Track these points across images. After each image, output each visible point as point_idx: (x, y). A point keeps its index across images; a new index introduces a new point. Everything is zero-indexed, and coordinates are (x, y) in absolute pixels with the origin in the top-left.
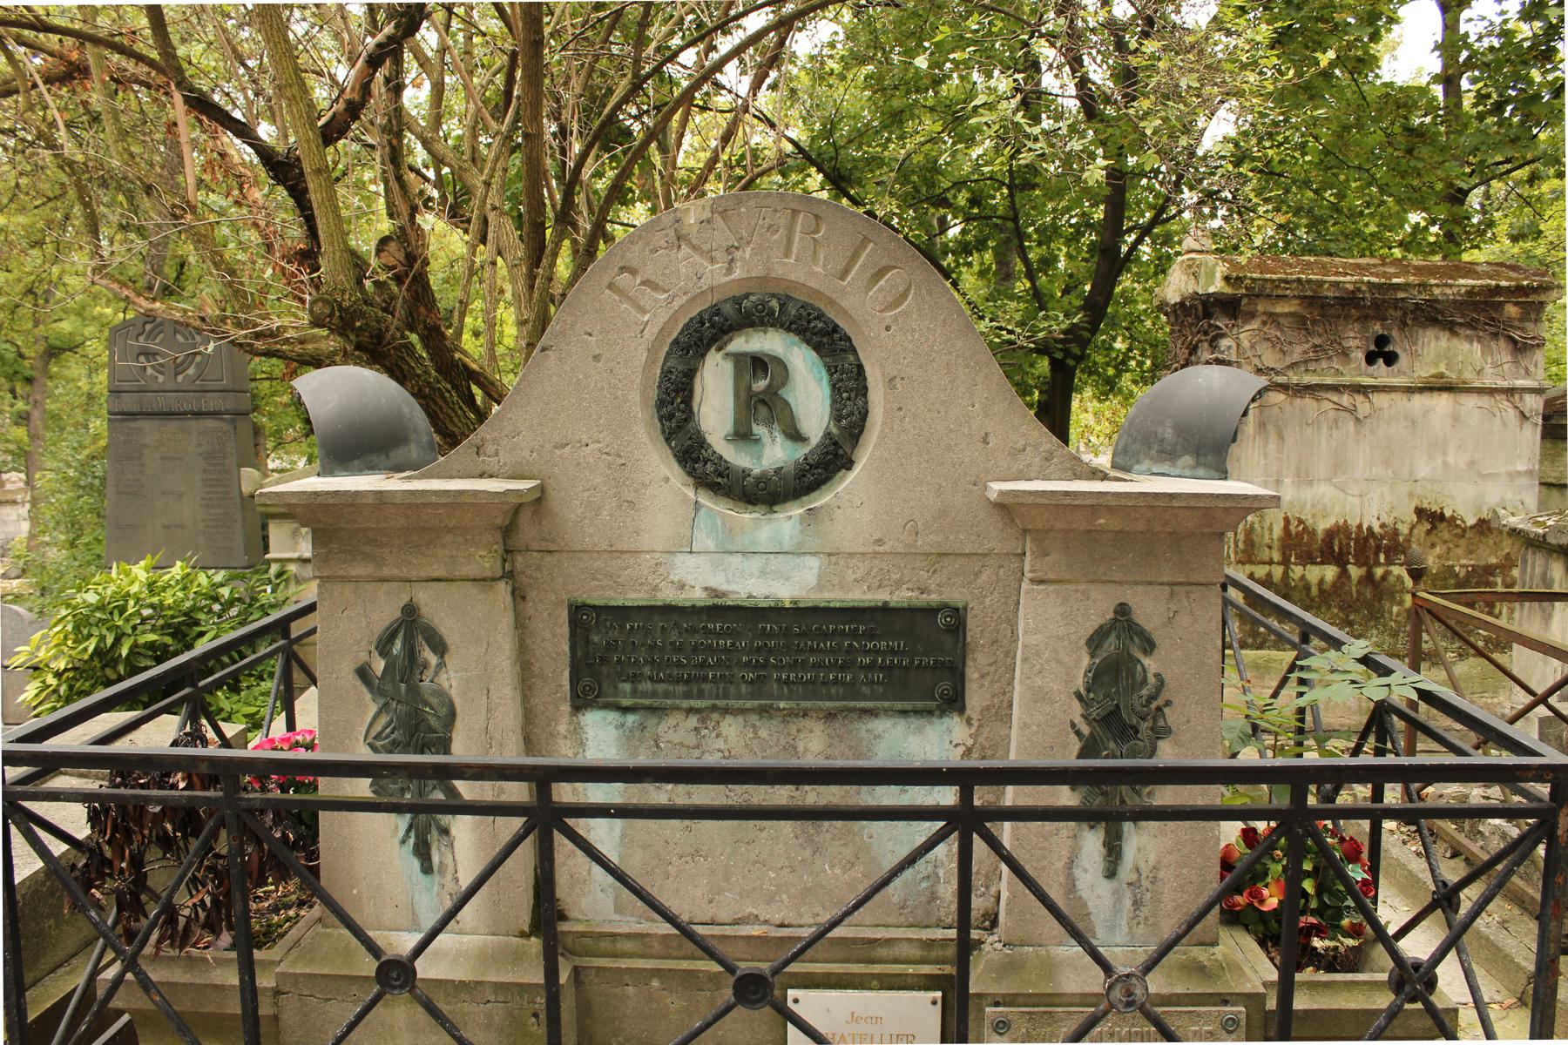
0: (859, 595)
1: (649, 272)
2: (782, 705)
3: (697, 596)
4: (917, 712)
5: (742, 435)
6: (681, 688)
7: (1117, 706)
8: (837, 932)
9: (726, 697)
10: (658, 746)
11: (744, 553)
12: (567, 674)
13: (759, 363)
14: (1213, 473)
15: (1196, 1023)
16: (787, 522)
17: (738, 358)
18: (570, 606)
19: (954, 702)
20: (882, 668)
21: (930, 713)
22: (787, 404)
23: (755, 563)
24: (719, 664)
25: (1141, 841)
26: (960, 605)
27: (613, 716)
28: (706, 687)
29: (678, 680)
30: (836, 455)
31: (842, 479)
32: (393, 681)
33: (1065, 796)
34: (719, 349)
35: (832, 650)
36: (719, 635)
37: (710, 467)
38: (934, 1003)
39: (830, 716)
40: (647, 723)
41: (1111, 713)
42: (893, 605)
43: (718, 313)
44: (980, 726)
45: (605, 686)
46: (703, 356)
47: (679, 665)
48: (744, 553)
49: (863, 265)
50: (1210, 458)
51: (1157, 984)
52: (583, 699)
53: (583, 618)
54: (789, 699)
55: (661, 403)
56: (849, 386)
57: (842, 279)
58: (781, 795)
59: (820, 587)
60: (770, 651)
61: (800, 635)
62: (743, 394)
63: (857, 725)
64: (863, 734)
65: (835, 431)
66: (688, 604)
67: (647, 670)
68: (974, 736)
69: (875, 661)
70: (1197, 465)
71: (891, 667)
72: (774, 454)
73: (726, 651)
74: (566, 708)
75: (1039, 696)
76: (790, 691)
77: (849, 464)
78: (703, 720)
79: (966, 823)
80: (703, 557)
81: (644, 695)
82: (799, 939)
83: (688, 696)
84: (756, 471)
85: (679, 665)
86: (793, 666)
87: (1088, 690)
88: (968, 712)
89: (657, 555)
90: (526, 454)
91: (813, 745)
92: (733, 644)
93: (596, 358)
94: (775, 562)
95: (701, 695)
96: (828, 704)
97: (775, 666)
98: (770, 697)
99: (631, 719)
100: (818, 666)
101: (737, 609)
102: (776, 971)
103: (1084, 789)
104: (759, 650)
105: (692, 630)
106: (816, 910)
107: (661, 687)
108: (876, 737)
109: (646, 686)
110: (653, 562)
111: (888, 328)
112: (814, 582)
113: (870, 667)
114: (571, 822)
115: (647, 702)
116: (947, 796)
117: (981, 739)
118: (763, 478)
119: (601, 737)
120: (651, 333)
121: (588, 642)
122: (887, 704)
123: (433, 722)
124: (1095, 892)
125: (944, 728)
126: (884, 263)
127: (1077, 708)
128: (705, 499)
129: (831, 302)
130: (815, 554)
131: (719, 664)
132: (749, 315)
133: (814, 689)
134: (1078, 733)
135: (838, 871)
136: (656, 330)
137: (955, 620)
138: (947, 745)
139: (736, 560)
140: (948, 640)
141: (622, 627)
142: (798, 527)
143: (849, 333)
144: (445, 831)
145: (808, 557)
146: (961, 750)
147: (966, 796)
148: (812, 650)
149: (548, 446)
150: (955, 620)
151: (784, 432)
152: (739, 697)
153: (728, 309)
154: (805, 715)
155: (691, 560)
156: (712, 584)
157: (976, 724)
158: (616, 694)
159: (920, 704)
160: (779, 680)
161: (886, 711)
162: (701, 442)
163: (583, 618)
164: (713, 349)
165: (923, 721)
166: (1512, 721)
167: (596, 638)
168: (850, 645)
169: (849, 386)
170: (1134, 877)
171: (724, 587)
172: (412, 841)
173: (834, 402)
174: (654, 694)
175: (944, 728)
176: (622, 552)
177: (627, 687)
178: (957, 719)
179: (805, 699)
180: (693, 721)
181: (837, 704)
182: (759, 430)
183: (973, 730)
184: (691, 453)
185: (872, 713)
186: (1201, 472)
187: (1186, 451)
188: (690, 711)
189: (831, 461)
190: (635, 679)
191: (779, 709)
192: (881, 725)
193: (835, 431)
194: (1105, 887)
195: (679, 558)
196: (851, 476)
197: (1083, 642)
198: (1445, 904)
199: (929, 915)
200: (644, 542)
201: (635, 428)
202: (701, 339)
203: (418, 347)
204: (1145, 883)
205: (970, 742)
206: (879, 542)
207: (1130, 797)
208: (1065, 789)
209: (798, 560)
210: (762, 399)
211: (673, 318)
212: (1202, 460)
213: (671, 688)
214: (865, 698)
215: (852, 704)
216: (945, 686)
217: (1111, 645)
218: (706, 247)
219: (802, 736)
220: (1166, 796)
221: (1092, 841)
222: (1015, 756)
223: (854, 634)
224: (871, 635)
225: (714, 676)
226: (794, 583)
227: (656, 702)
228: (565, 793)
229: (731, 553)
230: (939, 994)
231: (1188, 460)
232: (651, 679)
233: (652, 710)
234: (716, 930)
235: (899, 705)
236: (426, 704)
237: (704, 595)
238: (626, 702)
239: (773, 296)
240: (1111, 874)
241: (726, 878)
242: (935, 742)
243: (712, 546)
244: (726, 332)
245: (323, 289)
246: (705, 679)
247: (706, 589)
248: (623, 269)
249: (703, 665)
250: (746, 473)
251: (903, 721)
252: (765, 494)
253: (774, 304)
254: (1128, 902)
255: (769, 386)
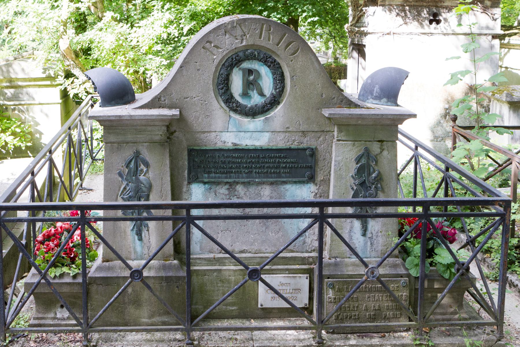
0: (281, 145)
1: (216, 43)
2: (257, 180)
3: (229, 146)
5: (245, 94)
6: (224, 175)
7: (365, 180)
8: (281, 255)
9: (238, 178)
11: (245, 132)
13: (250, 72)
14: (393, 104)
15: (393, 284)
16: (259, 122)
17: (244, 70)
18: (188, 150)
19: (312, 179)
20: (289, 168)
22: (259, 84)
23: (249, 134)
24: (237, 167)
25: (374, 225)
26: (314, 147)
27: (201, 185)
28: (232, 175)
29: (223, 173)
30: (275, 100)
31: (276, 107)
32: (131, 176)
33: (350, 210)
34: (238, 67)
35: (273, 163)
37: (234, 105)
38: (307, 278)
39: (272, 184)
41: (363, 182)
42: (292, 148)
43: (238, 56)
45: (199, 175)
46: (232, 69)
47: (223, 168)
49: (285, 41)
50: (392, 99)
51: (381, 271)
52: (193, 179)
53: (191, 152)
55: (218, 84)
56: (280, 79)
57: (278, 45)
58: (255, 211)
59: (269, 142)
60: (253, 163)
61: (263, 158)
62: (245, 81)
63: (280, 186)
65: (274, 93)
66: (227, 148)
67: (213, 170)
68: (318, 189)
69: (286, 166)
70: (388, 101)
71: (292, 168)
72: (256, 100)
73: (239, 163)
74: (186, 183)
75: (339, 178)
76: (259, 176)
77: (279, 103)
79: (321, 219)
80: (232, 133)
81: (212, 178)
82: (268, 257)
83: (226, 178)
84: (249, 106)
85: (223, 168)
86: (260, 168)
87: (356, 175)
90: (174, 100)
91: (266, 193)
92: (241, 161)
93: (198, 70)
94: (255, 134)
95: (230, 178)
96: (271, 180)
97: (255, 168)
98: (253, 178)
99: (207, 186)
101: (243, 149)
102: (262, 268)
103: (354, 208)
104: (249, 162)
105: (228, 157)
106: (266, 248)
107: (217, 175)
108: (286, 190)
111: (292, 61)
114: (197, 222)
115: (213, 180)
116: (316, 210)
117: (320, 190)
118: (252, 108)
119: (197, 193)
120: (216, 62)
121: (194, 161)
123: (144, 189)
124: (358, 240)
125: (308, 187)
126: (291, 40)
127: (353, 181)
128: (232, 114)
129: (273, 52)
130: (268, 132)
131: (237, 167)
132: (247, 57)
133: (267, 175)
134: (352, 189)
135: (273, 234)
136: (218, 61)
137: (313, 152)
138: (309, 193)
139: (242, 134)
140: (310, 159)
141: (205, 156)
142: (262, 124)
143: (280, 62)
144: (147, 226)
145: (265, 133)
146: (314, 194)
147: (321, 210)
148: (266, 163)
149: (182, 98)
151: (258, 93)
152: (243, 178)
153: (241, 54)
154: (264, 183)
155: (228, 134)
156: (235, 142)
160: (256, 172)
161: (290, 182)
162: (232, 97)
163: (191, 152)
164: (236, 67)
165: (302, 185)
166: (485, 180)
167: (196, 160)
169: (280, 79)
170: (371, 235)
171: (238, 143)
172: (135, 229)
173: (274, 83)
174: (215, 178)
177: (206, 175)
178: (312, 184)
181: (274, 179)
182: (250, 92)
183: (318, 187)
184: (229, 100)
185: (285, 183)
186: (389, 103)
187: (384, 97)
188: (227, 183)
189: (274, 102)
190: (209, 173)
191: (255, 182)
192: (288, 186)
193: (274, 93)
194: (362, 239)
195: (224, 133)
196: (279, 107)
197: (353, 160)
198: (470, 243)
199: (303, 249)
200: (213, 128)
201: (211, 92)
202: (232, 64)
204: (374, 237)
205: (316, 191)
206: (288, 128)
207: (370, 211)
208: (349, 208)
209: (262, 134)
210: (251, 83)
211: (224, 57)
212: (390, 100)
213: (221, 175)
214: (283, 178)
217: (363, 161)
218: (235, 35)
220: (381, 210)
221: (357, 224)
222: (332, 197)
223: (280, 157)
224: (285, 157)
225: (235, 171)
226: (262, 141)
227: (216, 180)
228: (195, 212)
230: (308, 275)
231: (385, 100)
232: (214, 173)
234: (244, 255)
235: (294, 180)
236: (142, 183)
238: (206, 180)
239: (255, 50)
240: (364, 235)
241: (237, 238)
242: (305, 192)
243: (235, 130)
244: (240, 62)
246: (232, 172)
248: (208, 42)
249: (231, 168)
250: (246, 106)
251: (295, 185)
252: (253, 113)
253: (256, 53)
254: (369, 243)
255: (254, 79)
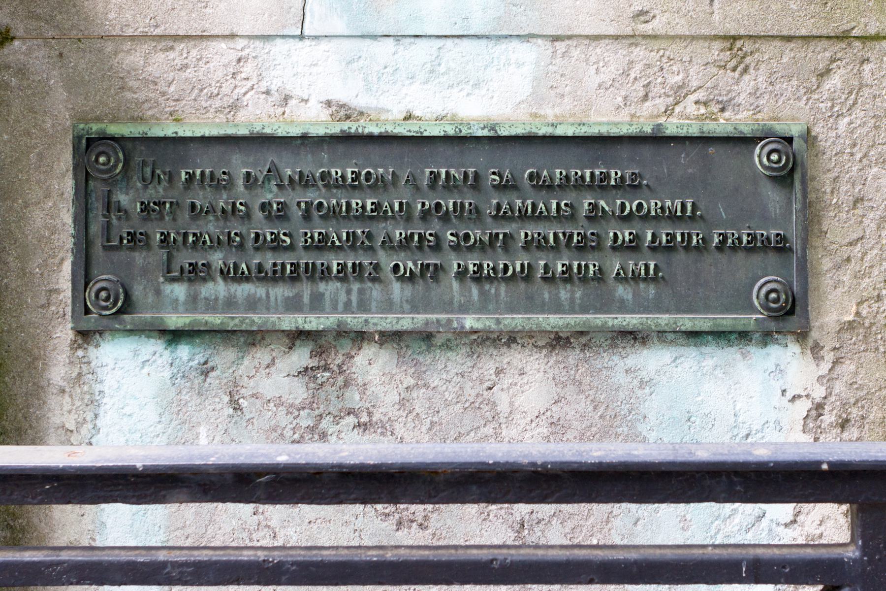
3: (311, 118)
4: (721, 336)
6: (280, 292)
9: (363, 307)
10: (237, 408)
12: (67, 267)
18: (77, 139)
19: (788, 316)
21: (743, 336)
26: (795, 130)
27: (153, 347)
29: (276, 276)
36: (355, 186)
39: (559, 341)
40: (215, 361)
44: (836, 362)
47: (277, 246)
48: (398, 38)
54: (482, 309)
64: (620, 378)
68: (827, 380)
73: (362, 217)
78: (320, 352)
80: (324, 45)
81: (211, 306)
83: (293, 305)
86: (487, 246)
88: (814, 334)
89: (240, 43)
98: (447, 306)
99: (184, 351)
100: (532, 245)
107: (243, 290)
108: (642, 384)
109: (218, 288)
110: (233, 56)
112: (528, 90)
113: (633, 246)
117: (839, 387)
122: (664, 319)
150: (793, 164)
152: (388, 307)
155: (303, 51)
156: (341, 95)
157: (829, 357)
158: (158, 306)
159: (727, 320)
161: (661, 334)
168: (594, 207)
174: (230, 304)
175: (770, 365)
176: (177, 38)
177: (179, 291)
178: (794, 348)
179: (512, 310)
180: (301, 357)
183: (825, 367)
203: (568, 553)
205: (819, 393)
214: (623, 308)
215: (598, 319)
216: (765, 283)
219: (506, 381)
225: (342, 268)
229: (374, 37)
232: (224, 274)
233: (223, 335)
237: (324, 115)
238: (175, 320)
245: (502, 326)
246: (325, 274)
247: (329, 103)
